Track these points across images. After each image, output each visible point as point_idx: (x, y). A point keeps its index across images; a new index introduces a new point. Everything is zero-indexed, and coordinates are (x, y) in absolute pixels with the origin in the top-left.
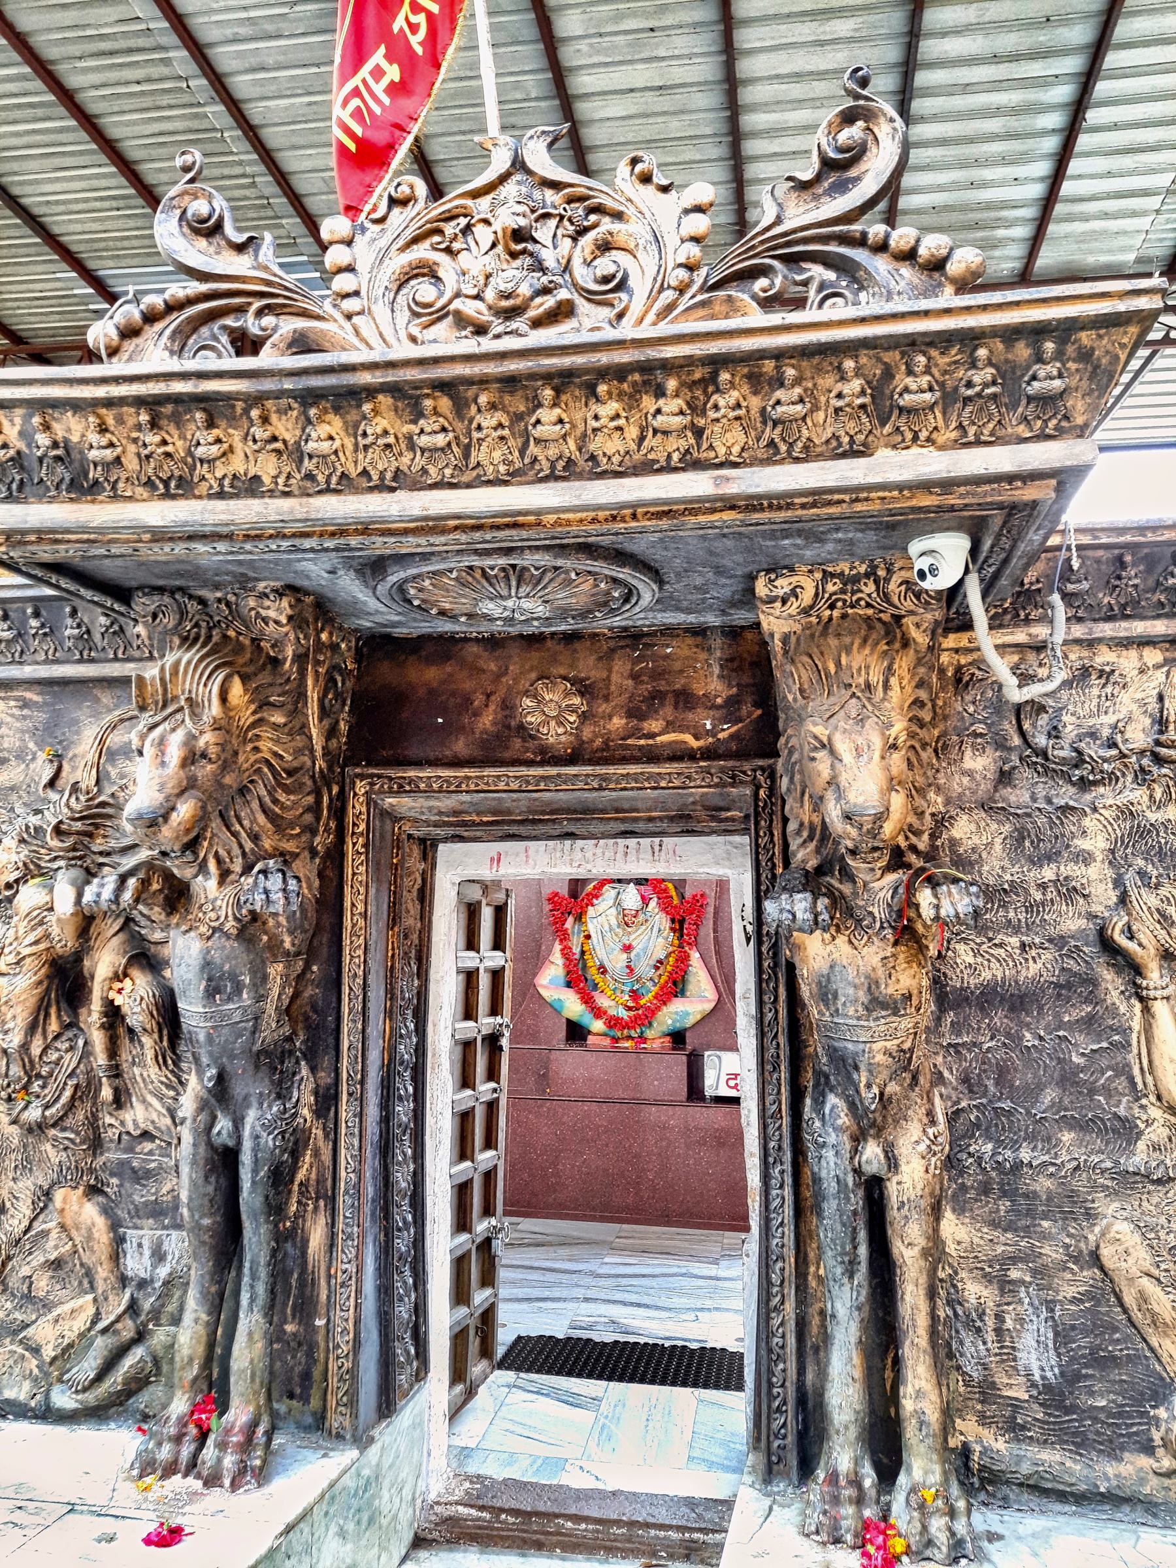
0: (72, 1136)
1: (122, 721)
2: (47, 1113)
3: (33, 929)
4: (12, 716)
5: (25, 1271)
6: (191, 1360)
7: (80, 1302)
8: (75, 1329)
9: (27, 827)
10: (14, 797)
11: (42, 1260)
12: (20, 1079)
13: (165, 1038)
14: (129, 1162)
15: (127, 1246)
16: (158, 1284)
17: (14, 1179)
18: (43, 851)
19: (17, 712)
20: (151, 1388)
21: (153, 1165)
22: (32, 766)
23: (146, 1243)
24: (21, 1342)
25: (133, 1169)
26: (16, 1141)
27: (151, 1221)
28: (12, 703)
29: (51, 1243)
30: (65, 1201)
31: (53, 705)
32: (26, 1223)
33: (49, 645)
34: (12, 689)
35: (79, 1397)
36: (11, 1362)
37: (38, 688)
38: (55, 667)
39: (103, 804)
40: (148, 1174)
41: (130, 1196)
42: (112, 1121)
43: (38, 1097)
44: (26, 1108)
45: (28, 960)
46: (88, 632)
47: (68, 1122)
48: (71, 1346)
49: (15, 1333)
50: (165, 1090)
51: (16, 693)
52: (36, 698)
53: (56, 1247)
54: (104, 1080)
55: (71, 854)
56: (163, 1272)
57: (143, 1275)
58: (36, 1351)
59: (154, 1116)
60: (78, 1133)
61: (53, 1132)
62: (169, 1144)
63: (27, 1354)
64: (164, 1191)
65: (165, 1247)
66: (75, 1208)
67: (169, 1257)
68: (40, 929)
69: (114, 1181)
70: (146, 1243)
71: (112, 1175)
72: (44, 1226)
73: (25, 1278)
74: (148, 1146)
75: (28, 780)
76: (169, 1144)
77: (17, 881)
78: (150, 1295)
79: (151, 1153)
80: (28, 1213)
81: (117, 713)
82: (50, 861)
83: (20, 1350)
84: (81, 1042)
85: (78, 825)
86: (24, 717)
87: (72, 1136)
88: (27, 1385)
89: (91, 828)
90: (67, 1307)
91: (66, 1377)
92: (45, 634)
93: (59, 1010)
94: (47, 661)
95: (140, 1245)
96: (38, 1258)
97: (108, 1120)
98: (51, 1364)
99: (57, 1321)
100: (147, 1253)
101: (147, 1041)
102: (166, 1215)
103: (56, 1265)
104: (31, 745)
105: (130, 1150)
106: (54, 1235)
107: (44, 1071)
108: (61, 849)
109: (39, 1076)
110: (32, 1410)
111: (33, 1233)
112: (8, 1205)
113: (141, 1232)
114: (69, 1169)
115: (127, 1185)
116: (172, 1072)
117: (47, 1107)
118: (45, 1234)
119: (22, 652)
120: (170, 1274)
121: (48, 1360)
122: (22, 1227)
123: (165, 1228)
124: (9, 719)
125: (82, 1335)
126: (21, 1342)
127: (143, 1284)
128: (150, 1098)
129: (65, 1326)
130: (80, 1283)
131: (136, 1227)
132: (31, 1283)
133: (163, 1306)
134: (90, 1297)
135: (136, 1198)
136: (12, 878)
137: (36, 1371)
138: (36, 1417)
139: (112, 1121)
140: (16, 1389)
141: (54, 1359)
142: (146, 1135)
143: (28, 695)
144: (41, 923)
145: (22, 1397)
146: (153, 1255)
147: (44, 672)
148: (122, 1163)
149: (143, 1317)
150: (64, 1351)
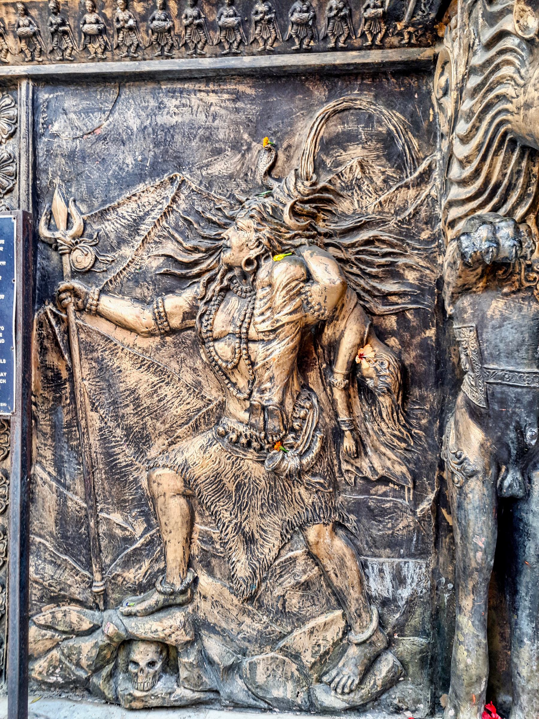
0: (322, 481)
1: (335, 112)
2: (304, 462)
3: (291, 299)
4: (226, 108)
5: (278, 591)
6: (479, 679)
7: (330, 616)
8: (329, 638)
9: (265, 207)
10: (233, 184)
11: (293, 582)
12: (279, 431)
13: (400, 398)
14: (365, 502)
15: (369, 571)
16: (401, 603)
17: (262, 516)
18: (283, 230)
19: (230, 105)
20: (401, 686)
21: (388, 505)
22: (248, 156)
23: (387, 569)
24: (281, 650)
25: (369, 507)
26: (263, 483)
27: (387, 550)
28: (226, 96)
29: (299, 568)
30: (319, 535)
31: (267, 97)
32: (275, 551)
33: (271, 33)
34: (225, 81)
35: (346, 697)
36: (274, 666)
37: (250, 82)
38: (274, 57)
39: (325, 189)
40: (384, 512)
41: (368, 530)
42: (349, 467)
43: (292, 447)
44: (283, 458)
45: (287, 327)
46: (314, 18)
47: (317, 469)
48: (326, 653)
49: (275, 642)
50: (396, 442)
51: (231, 87)
52: (249, 91)
53: (304, 572)
54: (347, 433)
55: (308, 233)
56: (405, 593)
57: (385, 595)
58: (296, 657)
59: (389, 464)
60: (325, 479)
61: (307, 478)
62: (403, 487)
63: (287, 659)
64: (401, 526)
65: (405, 571)
66: (328, 541)
67: (409, 581)
68: (298, 300)
69: (352, 517)
70: (387, 569)
71: (350, 512)
72: (291, 554)
73: (279, 597)
74: (382, 489)
75: (244, 170)
76: (403, 487)
77: (258, 258)
78: (394, 612)
79: (385, 494)
80: (277, 543)
81: (332, 104)
82: (290, 239)
83: (280, 657)
84: (315, 401)
85: (308, 207)
86: (237, 110)
87: (322, 481)
88: (290, 686)
89: (315, 211)
90: (321, 620)
91: (325, 679)
92: (269, 21)
93: (297, 375)
94: (265, 52)
95: (381, 571)
96: (288, 581)
97: (345, 466)
98: (311, 668)
99: (312, 632)
100: (388, 577)
101: (385, 401)
102: (401, 546)
103: (306, 586)
104: (246, 136)
105: (366, 492)
106: (301, 561)
107: (296, 425)
108: (299, 228)
109: (293, 430)
110: (299, 706)
111: (282, 559)
112: (257, 536)
113: (381, 560)
114: (321, 508)
115: (364, 520)
116: (404, 426)
117: (301, 456)
118: (293, 560)
119: (241, 42)
120: (412, 595)
121: (309, 665)
122: (273, 554)
123: (401, 556)
124: (223, 112)
125: (335, 644)
126: (281, 650)
127: (385, 603)
128: (383, 449)
129: (319, 637)
130: (328, 601)
131: (374, 556)
132: (285, 601)
133: (407, 620)
134: (339, 613)
135: (374, 532)
136: (253, 254)
137: (296, 673)
138: (301, 710)
139: (349, 467)
140: (281, 689)
141: (314, 664)
142: (384, 480)
143: (241, 88)
144: (299, 293)
145: (289, 696)
146: (394, 579)
147: (264, 62)
148: (358, 503)
149: (389, 629)
150: (322, 656)
